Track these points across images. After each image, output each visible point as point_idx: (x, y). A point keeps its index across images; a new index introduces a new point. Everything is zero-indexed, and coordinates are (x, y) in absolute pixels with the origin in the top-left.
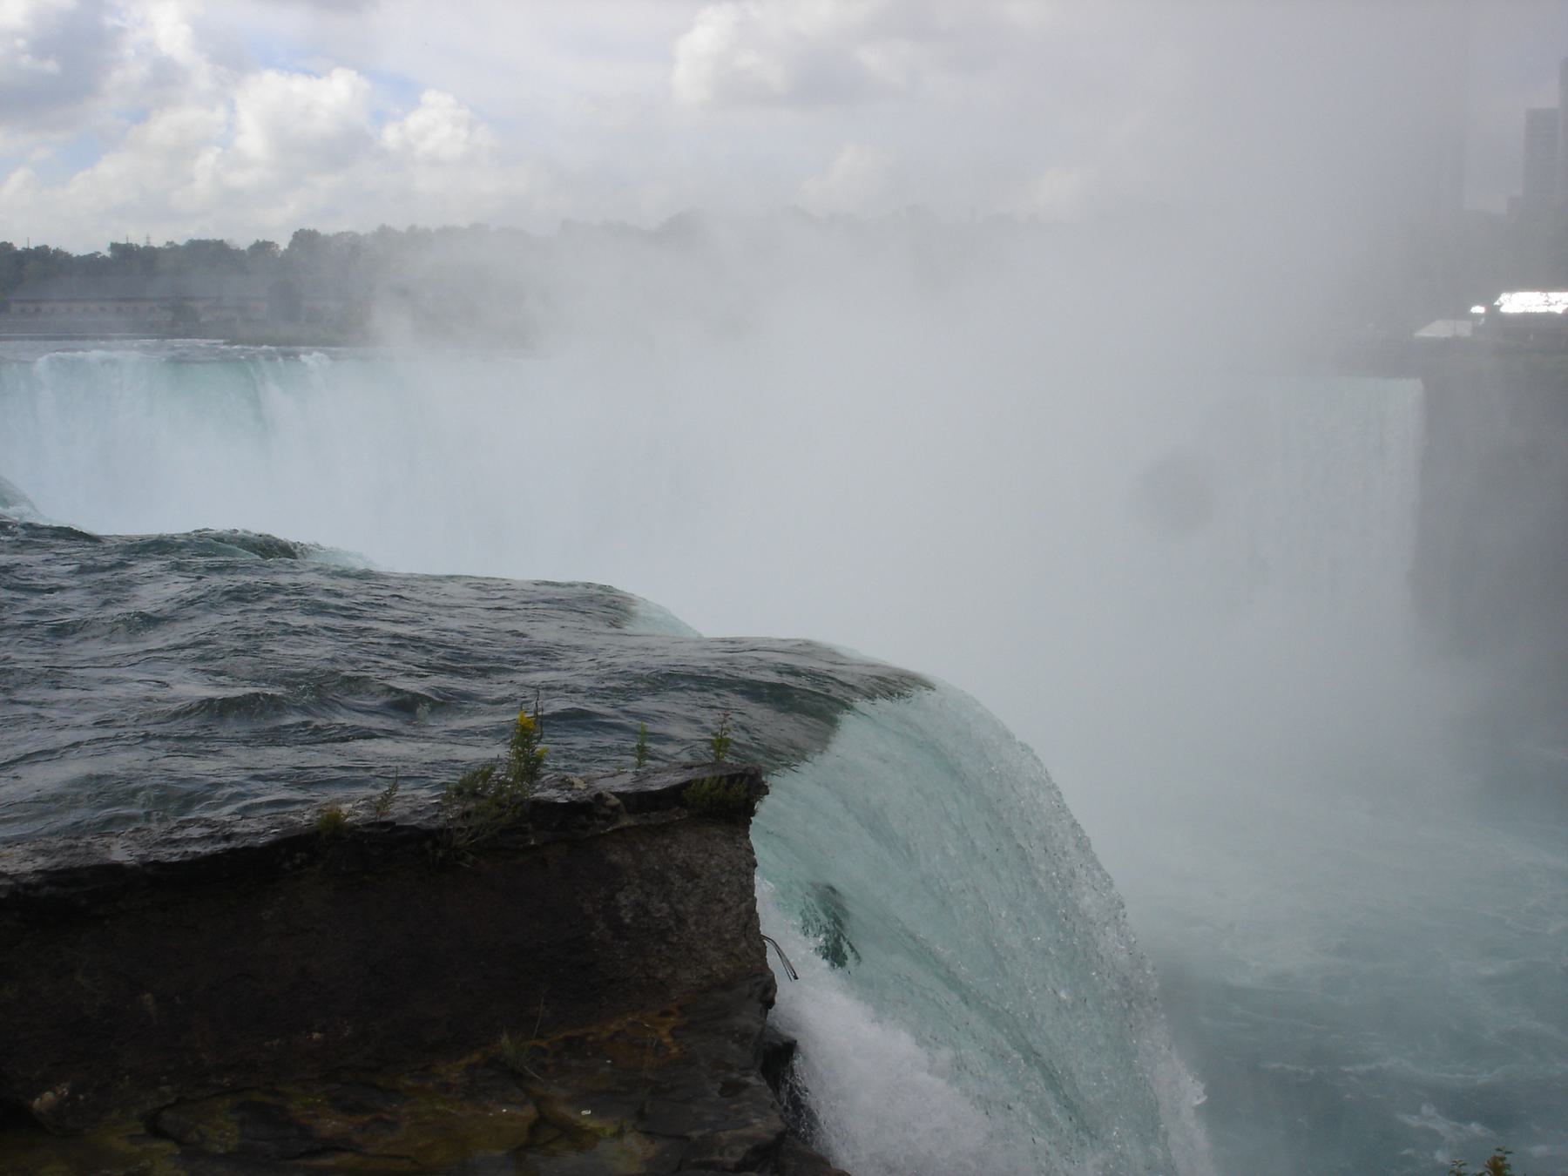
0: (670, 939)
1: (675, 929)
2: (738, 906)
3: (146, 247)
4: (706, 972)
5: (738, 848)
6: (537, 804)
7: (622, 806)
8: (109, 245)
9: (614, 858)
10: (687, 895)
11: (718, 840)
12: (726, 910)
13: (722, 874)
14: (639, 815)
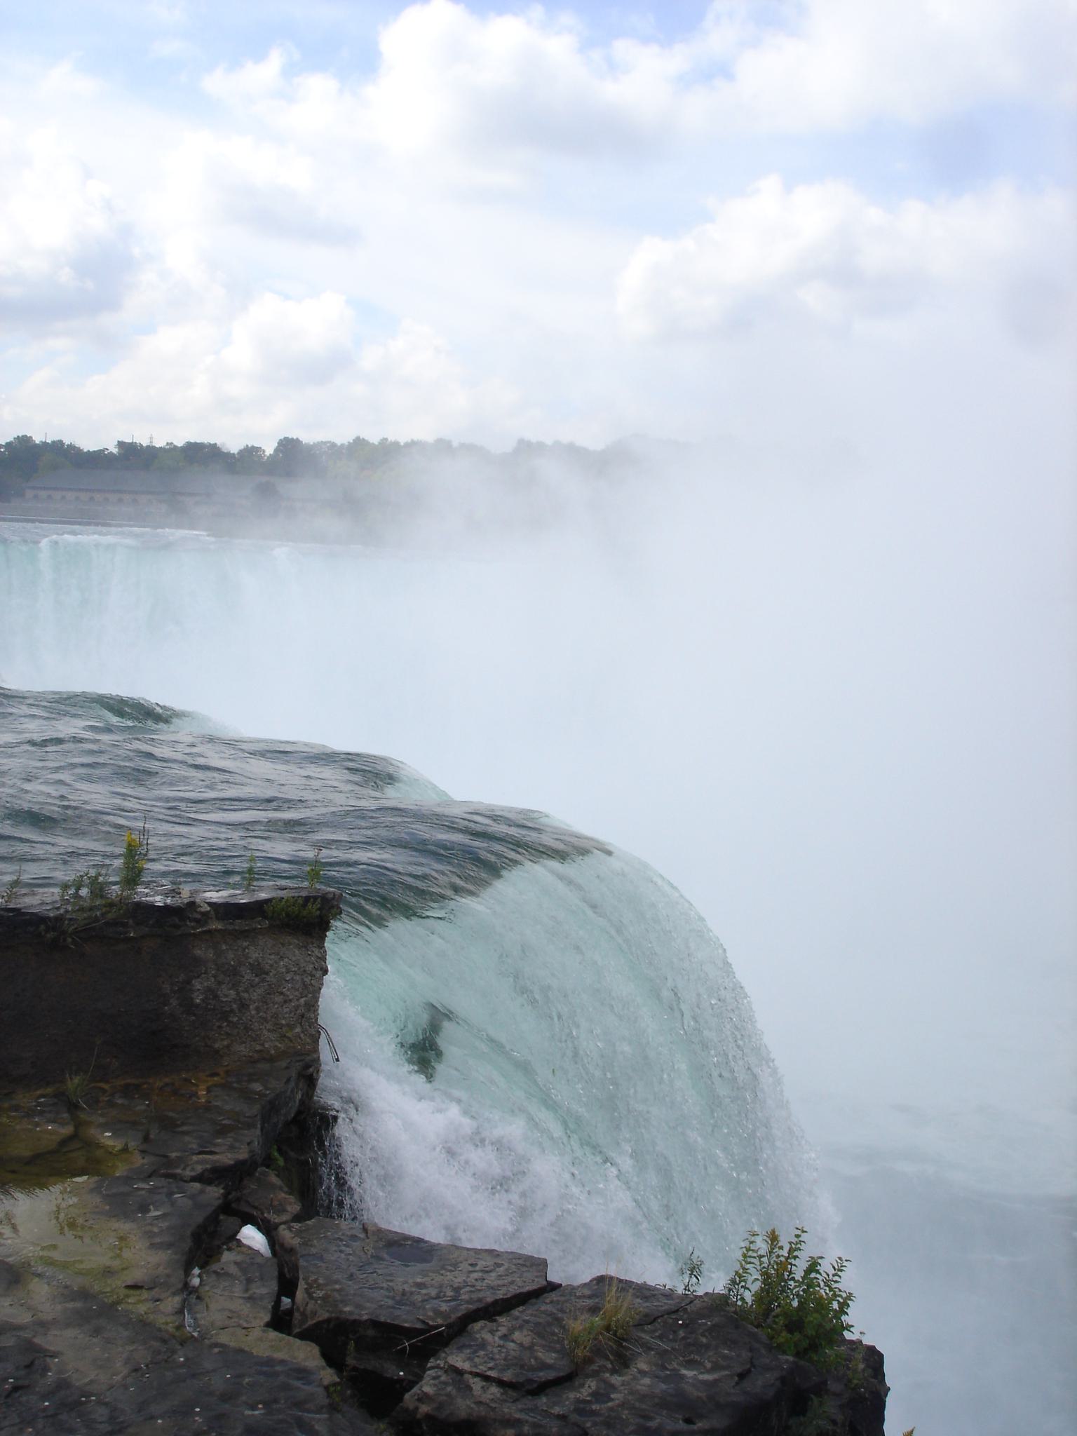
0: (231, 1019)
1: (237, 1011)
2: (297, 1000)
3: (148, 446)
4: (258, 1048)
5: (309, 955)
6: (139, 905)
7: (212, 913)
8: (116, 443)
9: (198, 952)
10: (252, 986)
11: (291, 947)
12: (285, 1002)
13: (287, 973)
14: (226, 922)
